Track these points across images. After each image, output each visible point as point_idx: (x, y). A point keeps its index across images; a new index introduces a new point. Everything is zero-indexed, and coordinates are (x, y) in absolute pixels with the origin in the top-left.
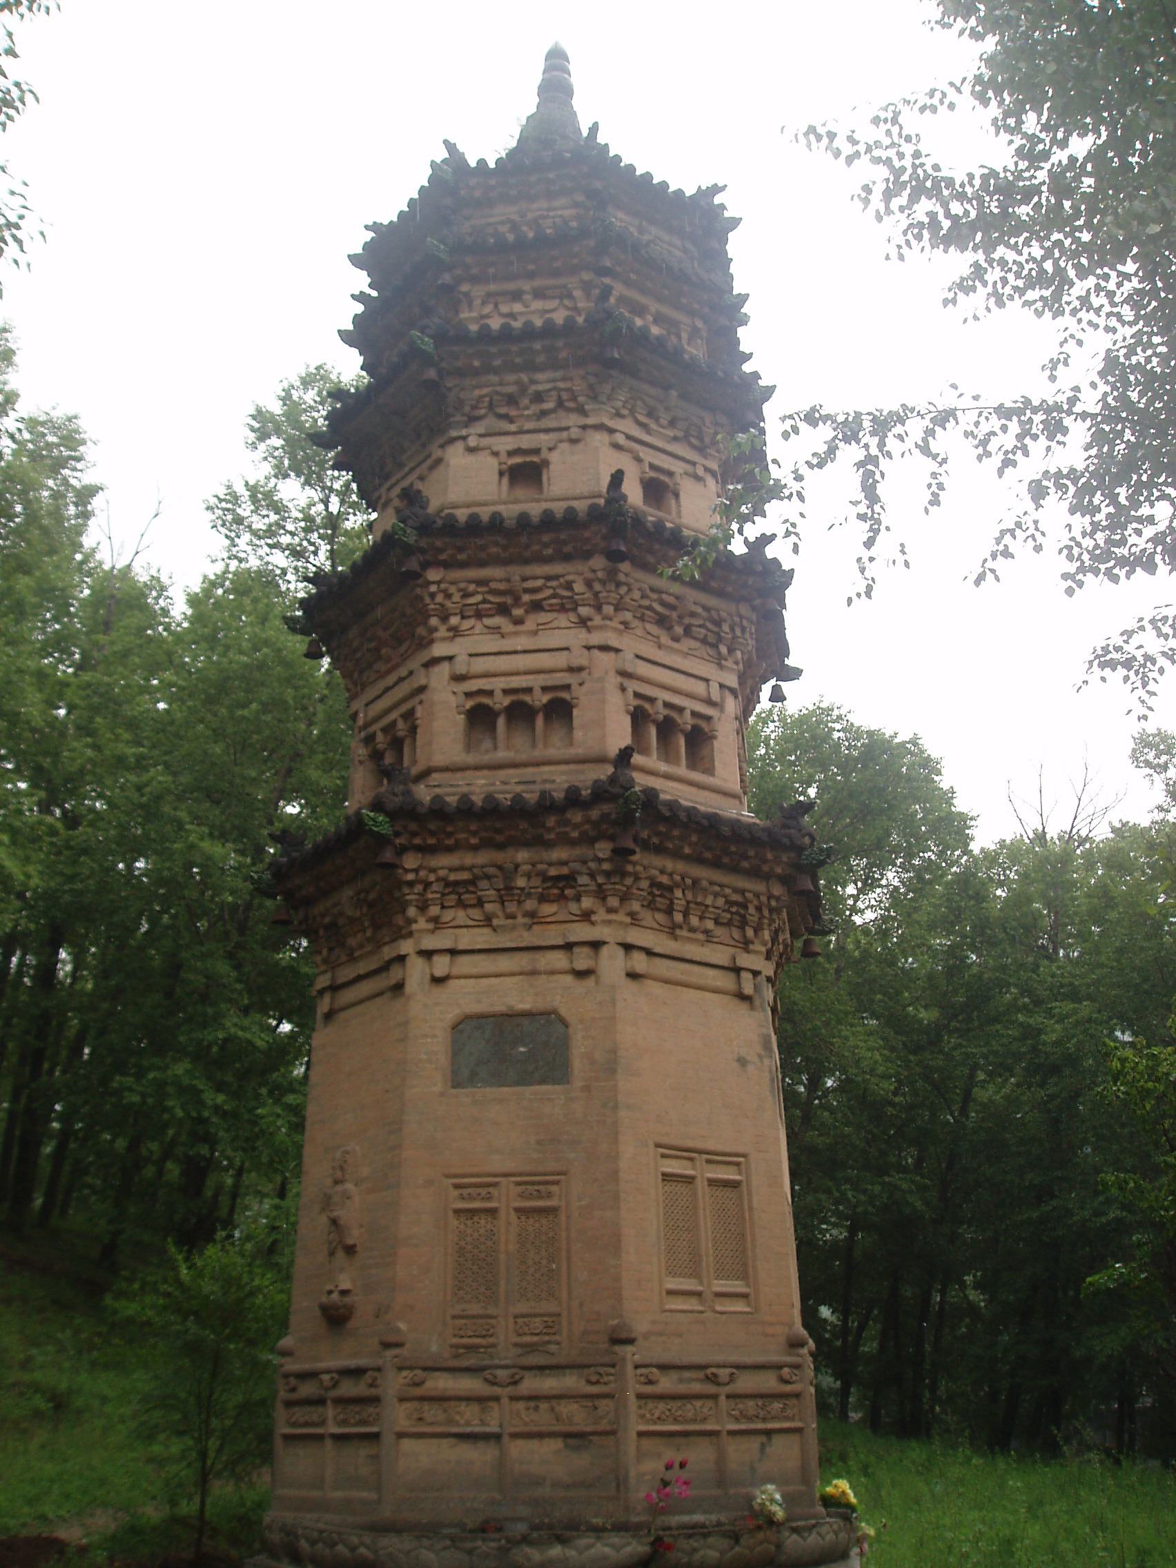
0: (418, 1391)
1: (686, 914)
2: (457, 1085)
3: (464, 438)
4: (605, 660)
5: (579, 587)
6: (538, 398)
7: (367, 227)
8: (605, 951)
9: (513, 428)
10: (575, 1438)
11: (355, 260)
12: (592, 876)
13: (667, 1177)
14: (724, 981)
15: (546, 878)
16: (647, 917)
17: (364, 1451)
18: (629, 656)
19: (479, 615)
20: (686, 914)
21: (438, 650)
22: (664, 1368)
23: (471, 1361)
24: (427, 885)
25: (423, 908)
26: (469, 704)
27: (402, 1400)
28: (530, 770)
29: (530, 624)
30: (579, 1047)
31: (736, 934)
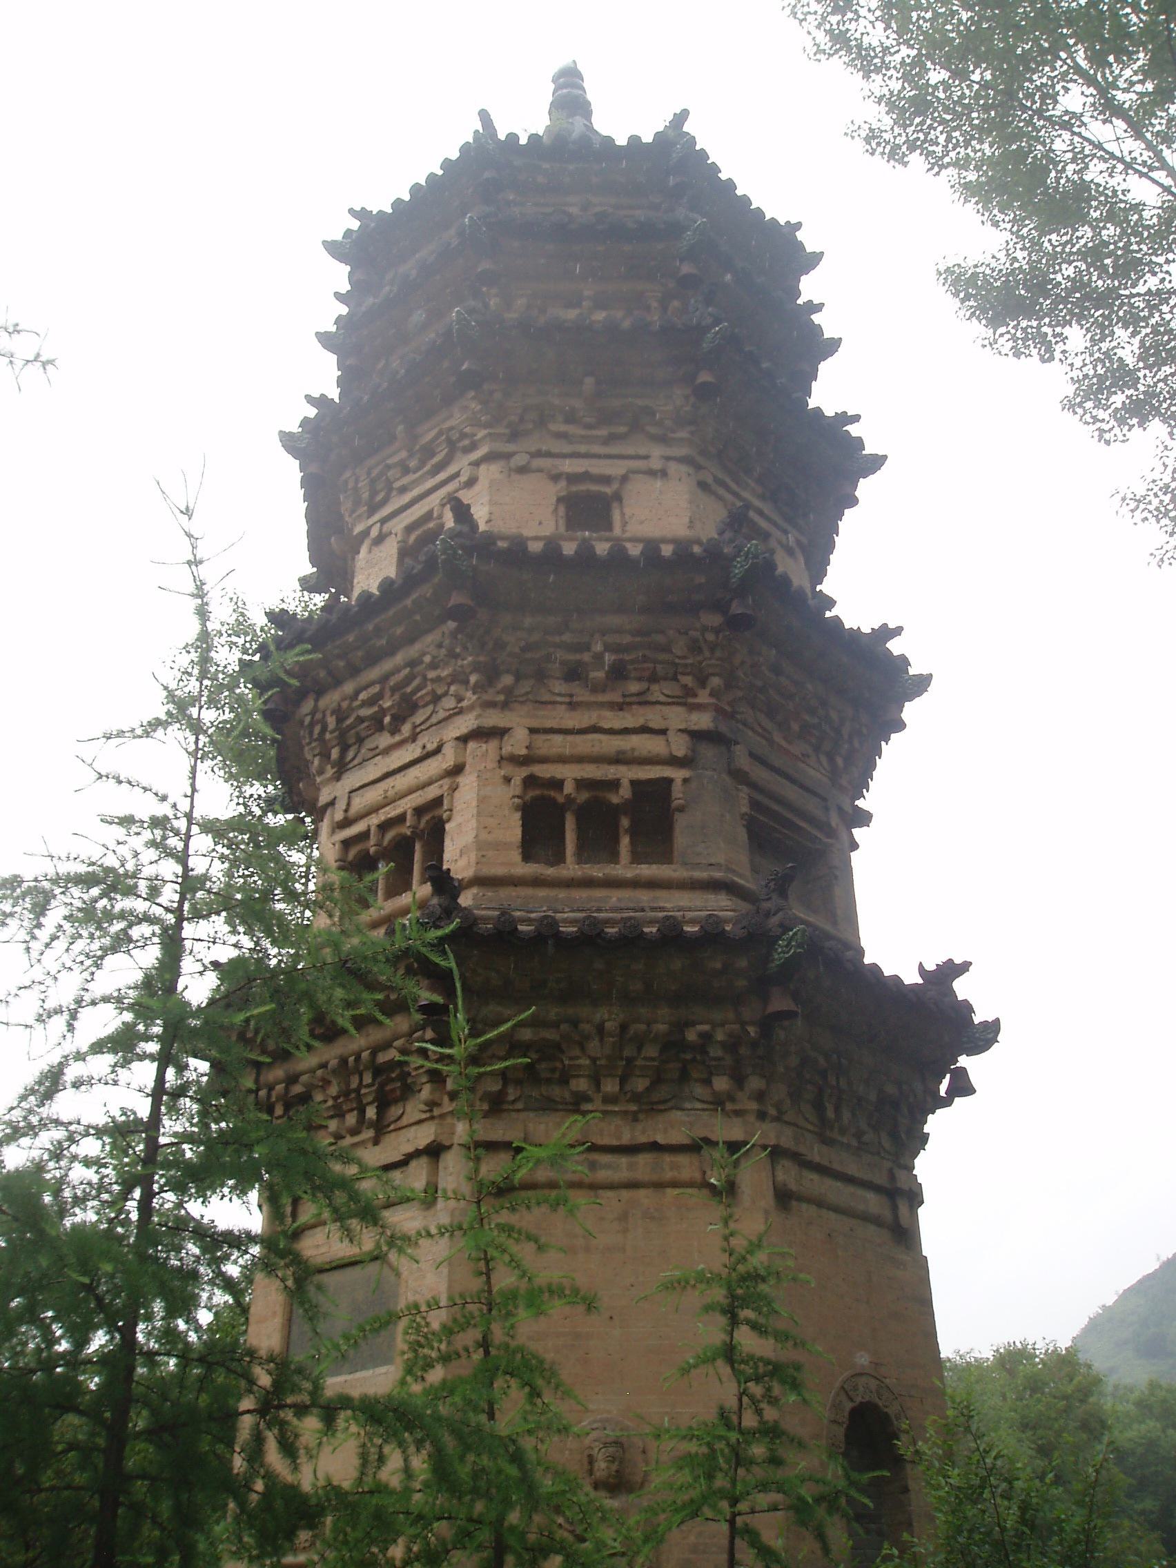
7: (309, 399)
11: (333, 248)
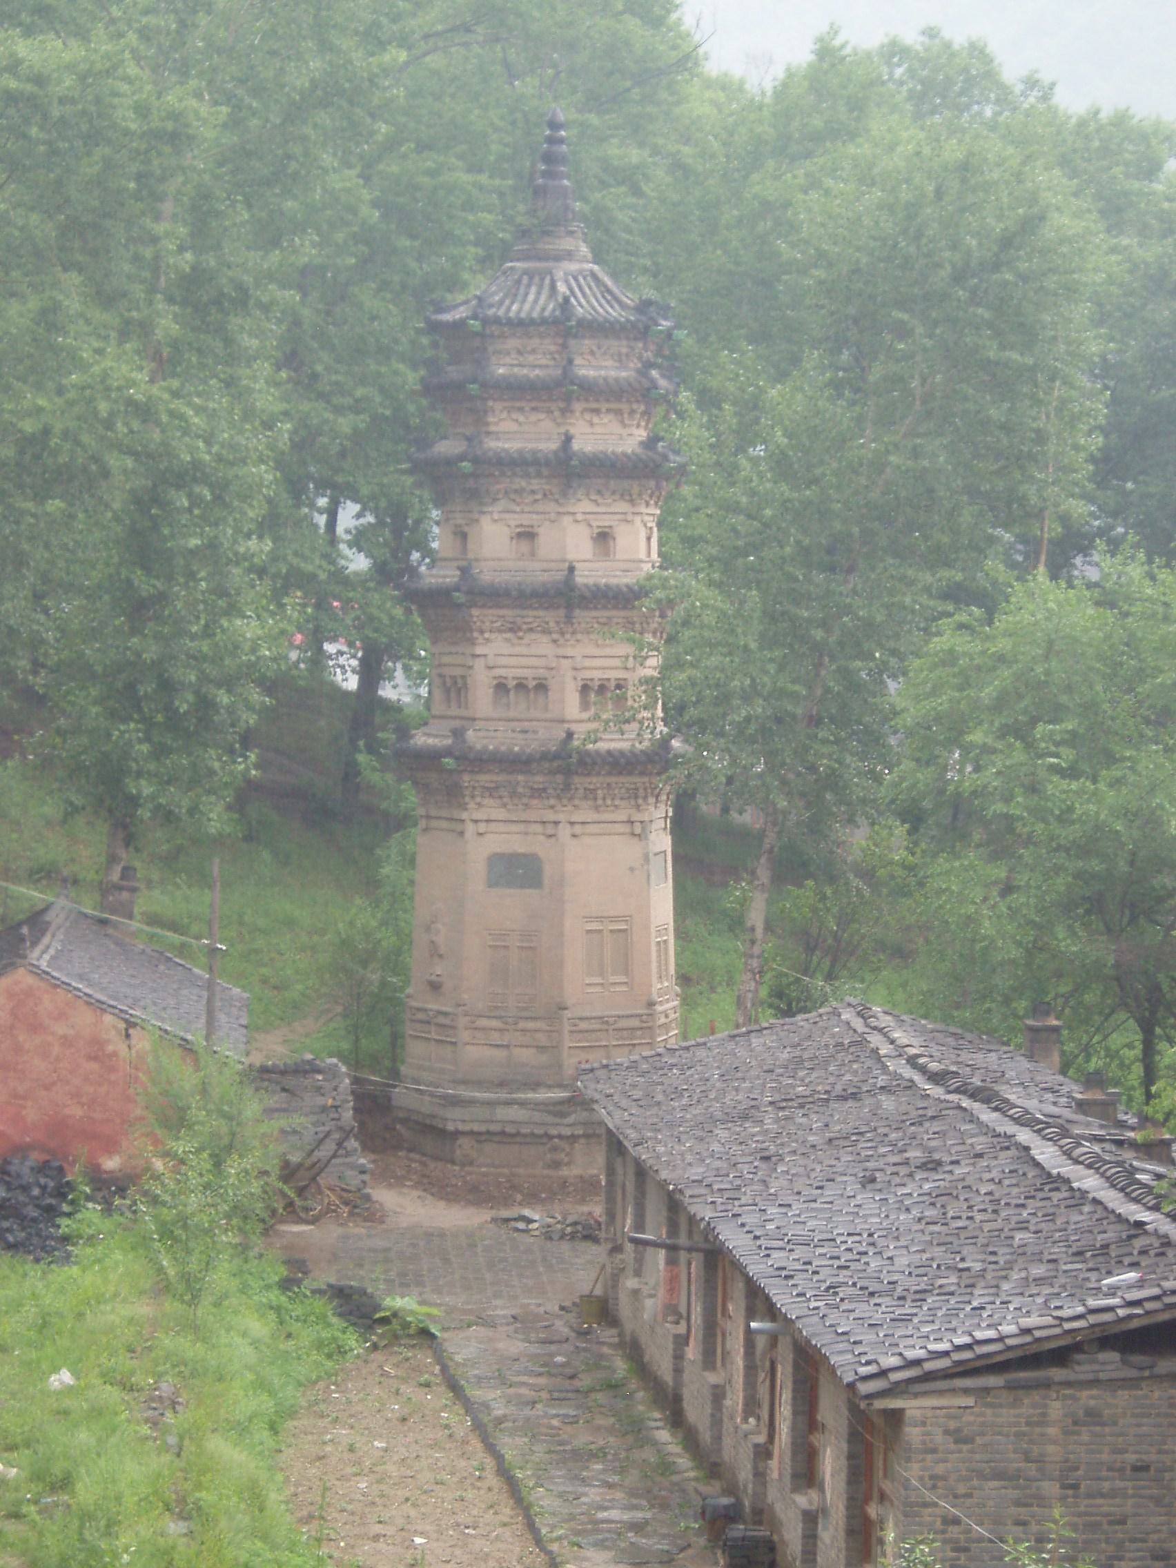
0: (474, 1026)
1: (604, 799)
2: (490, 886)
3: (491, 513)
4: (566, 663)
5: (552, 624)
6: (533, 492)
8: (561, 825)
9: (518, 509)
10: (541, 1049)
12: (555, 789)
13: (588, 932)
14: (625, 828)
15: (532, 788)
16: (585, 804)
17: (449, 1048)
18: (579, 659)
19: (500, 631)
20: (604, 799)
21: (479, 650)
22: (581, 1019)
23: (497, 1013)
24: (474, 788)
25: (473, 797)
26: (495, 682)
27: (466, 1029)
28: (526, 724)
29: (525, 641)
30: (548, 871)
31: (633, 802)
